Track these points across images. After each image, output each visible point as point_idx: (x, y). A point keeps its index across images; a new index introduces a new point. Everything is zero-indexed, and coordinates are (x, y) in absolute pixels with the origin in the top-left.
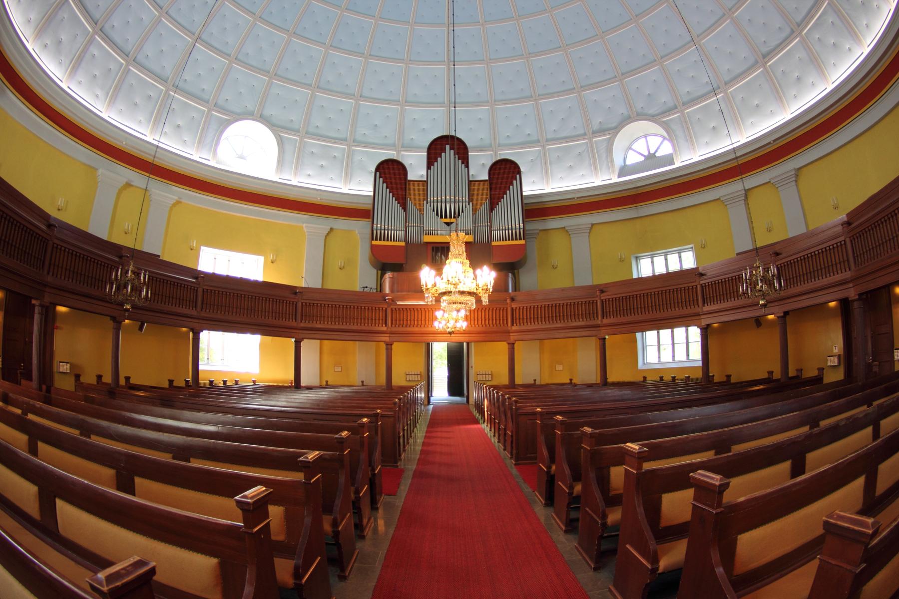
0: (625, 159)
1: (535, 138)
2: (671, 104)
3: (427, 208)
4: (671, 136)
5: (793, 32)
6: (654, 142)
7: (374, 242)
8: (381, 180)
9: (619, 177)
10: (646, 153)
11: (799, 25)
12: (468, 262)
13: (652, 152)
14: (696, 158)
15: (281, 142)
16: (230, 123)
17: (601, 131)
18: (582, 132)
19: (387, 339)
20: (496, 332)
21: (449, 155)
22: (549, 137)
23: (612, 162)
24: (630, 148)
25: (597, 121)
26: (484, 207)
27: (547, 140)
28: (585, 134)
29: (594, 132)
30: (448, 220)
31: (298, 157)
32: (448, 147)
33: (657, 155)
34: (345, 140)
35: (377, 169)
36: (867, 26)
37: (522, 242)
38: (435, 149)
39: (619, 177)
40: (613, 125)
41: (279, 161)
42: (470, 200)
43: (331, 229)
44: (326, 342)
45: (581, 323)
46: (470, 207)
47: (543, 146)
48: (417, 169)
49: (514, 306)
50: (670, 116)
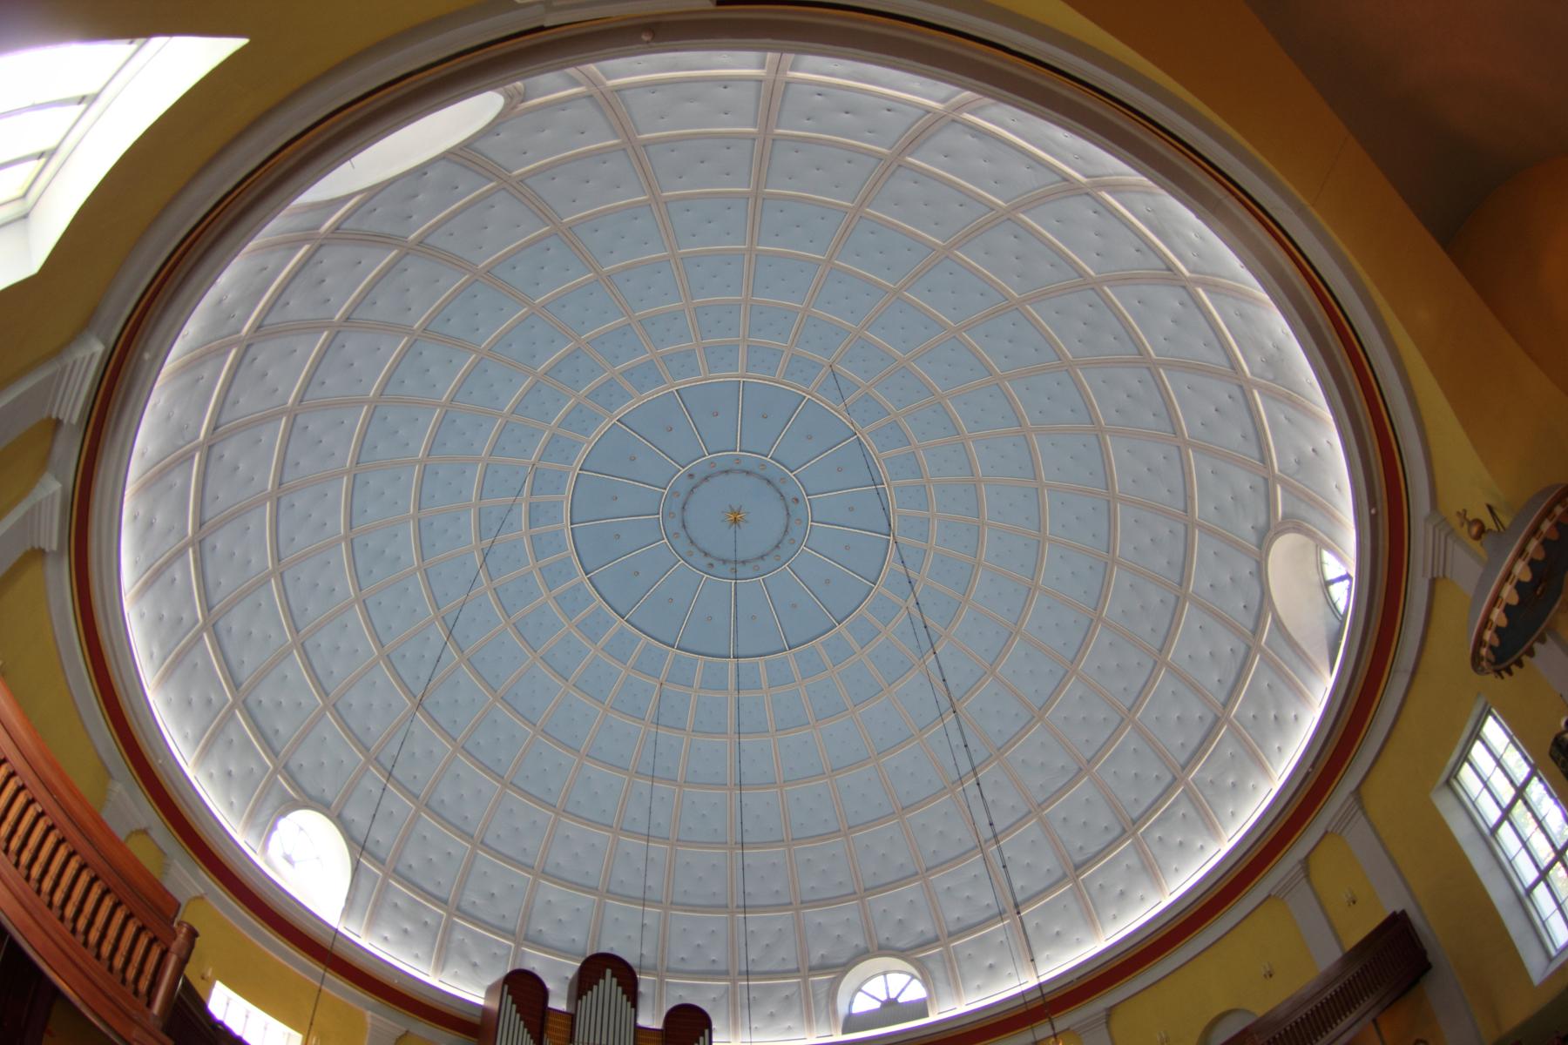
1: (723, 967)
2: (930, 935)
4: (925, 974)
5: (1124, 831)
10: (884, 997)
11: (1134, 822)
13: (893, 996)
14: (962, 1008)
15: (356, 869)
16: (295, 805)
21: (609, 984)
23: (835, 1012)
24: (859, 989)
25: (817, 954)
28: (798, 970)
32: (609, 972)
33: (900, 1000)
36: (1233, 814)
39: (845, 1032)
40: (843, 960)
47: (734, 982)
48: (558, 1003)
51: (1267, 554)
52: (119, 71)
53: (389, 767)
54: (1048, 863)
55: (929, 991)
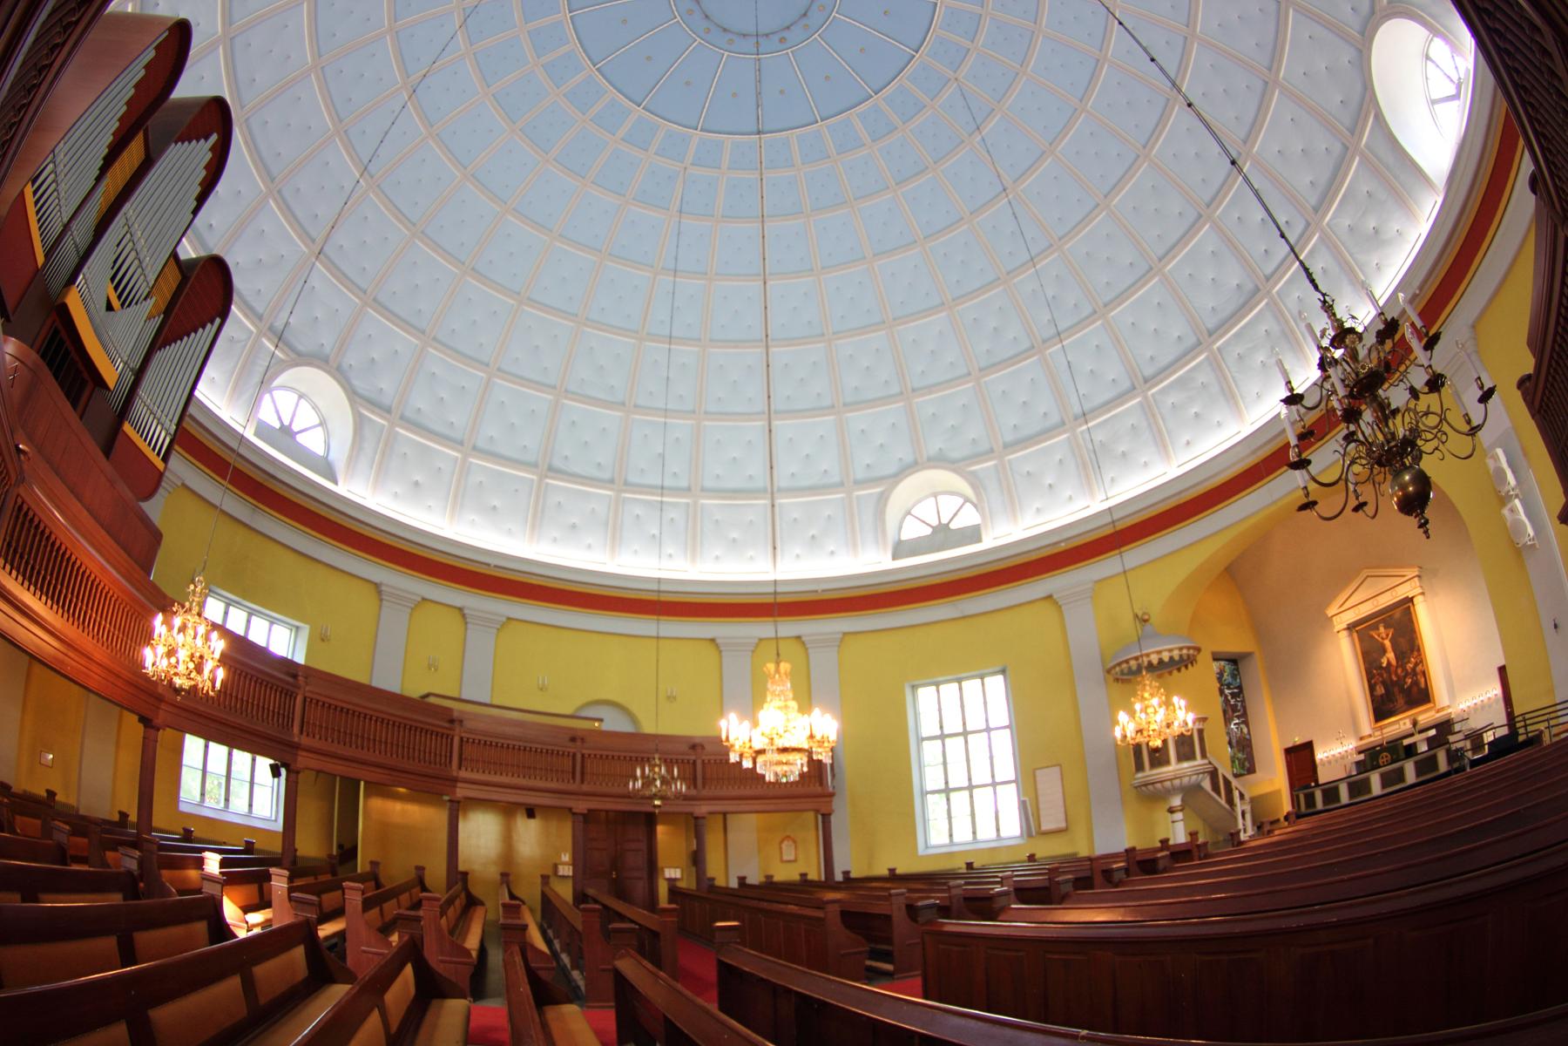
2: (386, 401)
6: (949, 505)
9: (894, 558)
10: (935, 523)
12: (793, 704)
13: (945, 521)
23: (884, 532)
24: (322, 423)
33: (952, 526)
39: (894, 558)
45: (553, 785)
50: (989, 464)
51: (329, 373)
53: (366, 161)
54: (1113, 370)
55: (983, 516)
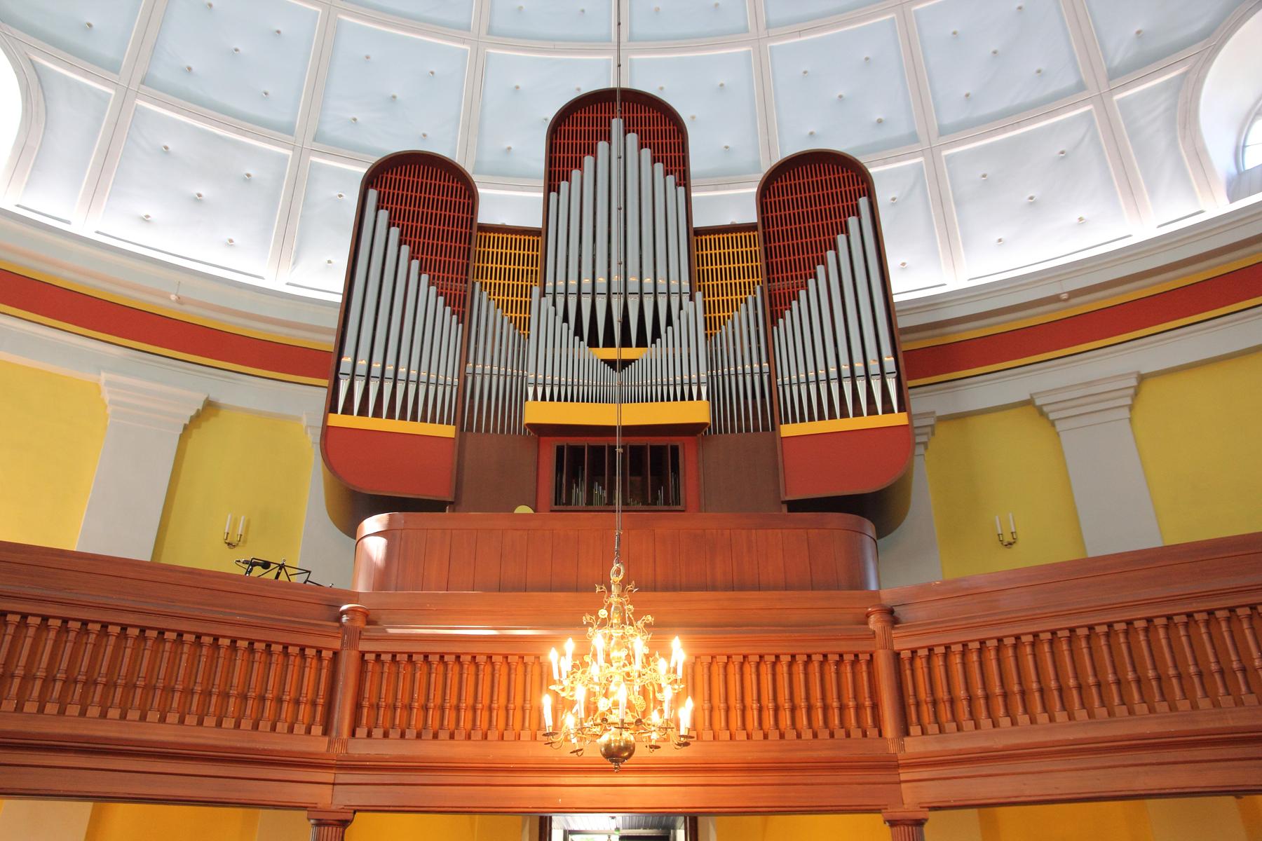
0: (1239, 152)
3: (544, 312)
7: (337, 420)
8: (384, 215)
9: (1232, 201)
17: (1145, 61)
18: (1069, 81)
19: (323, 796)
20: (833, 766)
21: (622, 149)
22: (948, 119)
23: (1199, 155)
26: (744, 317)
27: (942, 132)
28: (1081, 87)
29: (1113, 74)
30: (611, 353)
31: (107, 154)
32: (617, 125)
34: (289, 130)
35: (371, 180)
37: (899, 419)
38: (576, 130)
39: (1232, 201)
41: (21, 149)
42: (696, 278)
43: (210, 407)
44: (121, 811)
46: (692, 312)
47: (932, 153)
48: (509, 201)
49: (903, 644)
52: (595, 227)
